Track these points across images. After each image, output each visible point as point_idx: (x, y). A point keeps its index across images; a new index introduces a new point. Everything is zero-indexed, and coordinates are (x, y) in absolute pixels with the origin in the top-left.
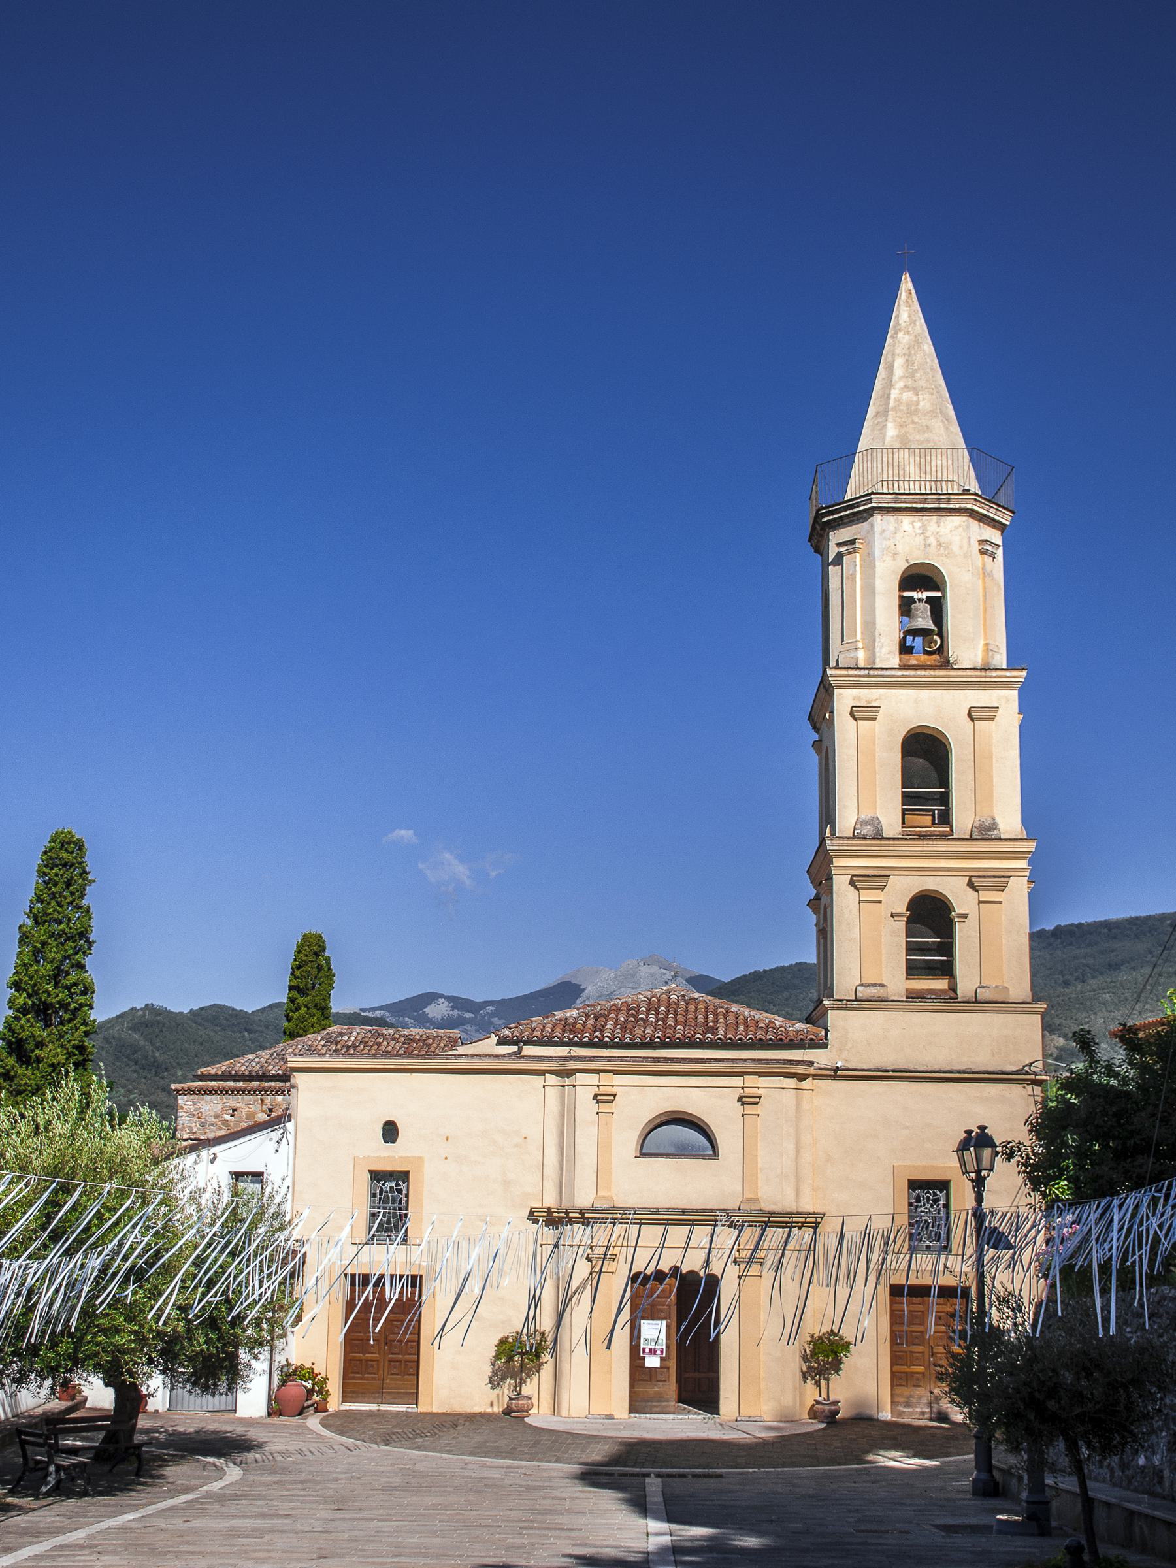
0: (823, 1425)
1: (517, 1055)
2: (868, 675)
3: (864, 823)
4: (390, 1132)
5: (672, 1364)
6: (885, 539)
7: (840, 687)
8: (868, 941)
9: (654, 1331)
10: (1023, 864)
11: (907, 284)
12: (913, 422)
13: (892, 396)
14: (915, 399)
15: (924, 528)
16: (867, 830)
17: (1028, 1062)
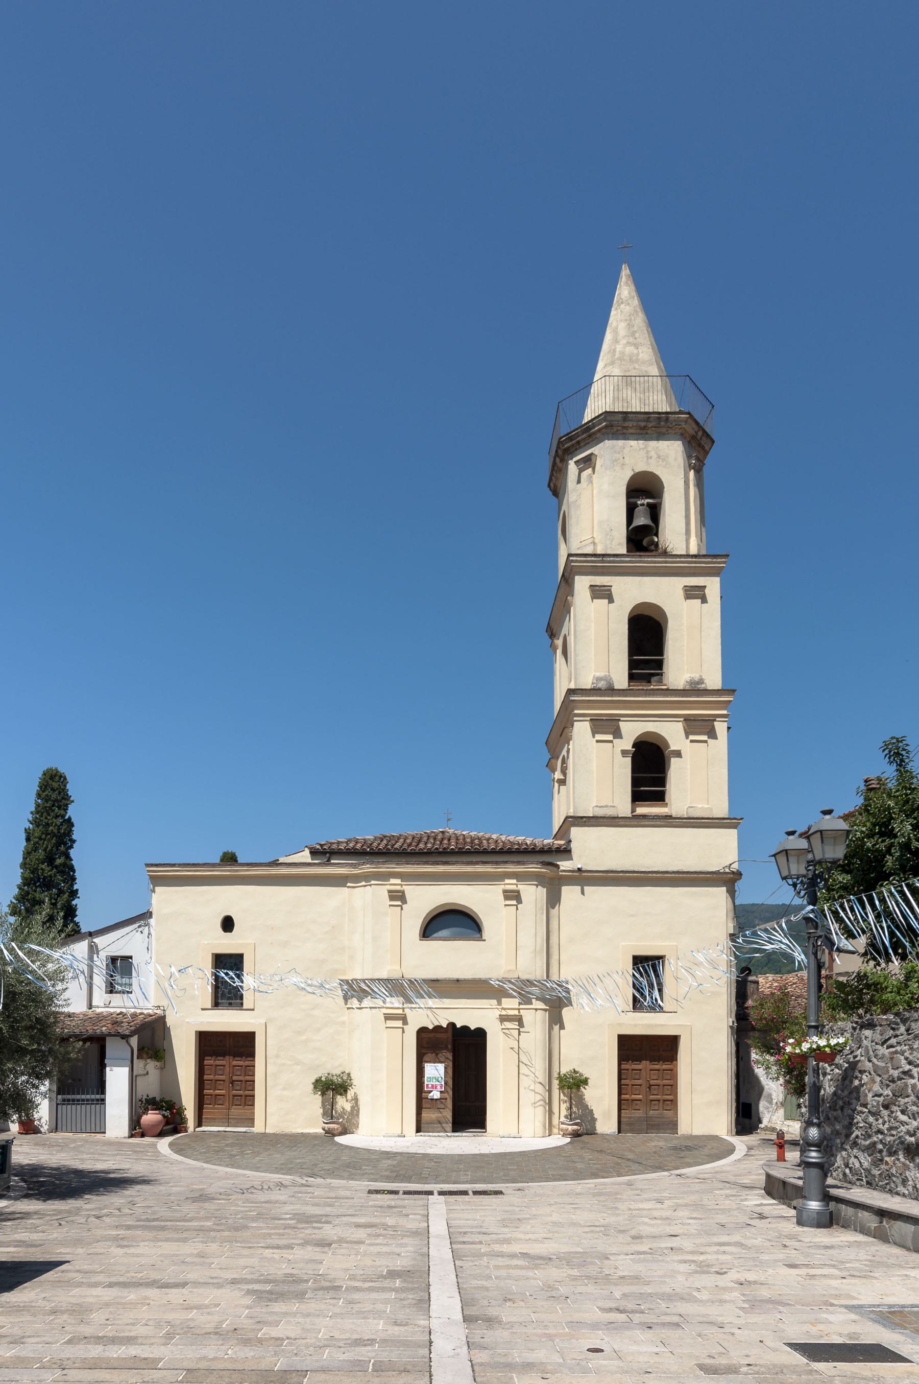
0: (568, 1140)
2: (603, 562)
3: (599, 679)
4: (228, 924)
5: (449, 1096)
6: (615, 452)
8: (596, 771)
9: (436, 1072)
11: (625, 272)
12: (635, 368)
13: (618, 350)
14: (636, 351)
16: (602, 685)
17: (728, 864)
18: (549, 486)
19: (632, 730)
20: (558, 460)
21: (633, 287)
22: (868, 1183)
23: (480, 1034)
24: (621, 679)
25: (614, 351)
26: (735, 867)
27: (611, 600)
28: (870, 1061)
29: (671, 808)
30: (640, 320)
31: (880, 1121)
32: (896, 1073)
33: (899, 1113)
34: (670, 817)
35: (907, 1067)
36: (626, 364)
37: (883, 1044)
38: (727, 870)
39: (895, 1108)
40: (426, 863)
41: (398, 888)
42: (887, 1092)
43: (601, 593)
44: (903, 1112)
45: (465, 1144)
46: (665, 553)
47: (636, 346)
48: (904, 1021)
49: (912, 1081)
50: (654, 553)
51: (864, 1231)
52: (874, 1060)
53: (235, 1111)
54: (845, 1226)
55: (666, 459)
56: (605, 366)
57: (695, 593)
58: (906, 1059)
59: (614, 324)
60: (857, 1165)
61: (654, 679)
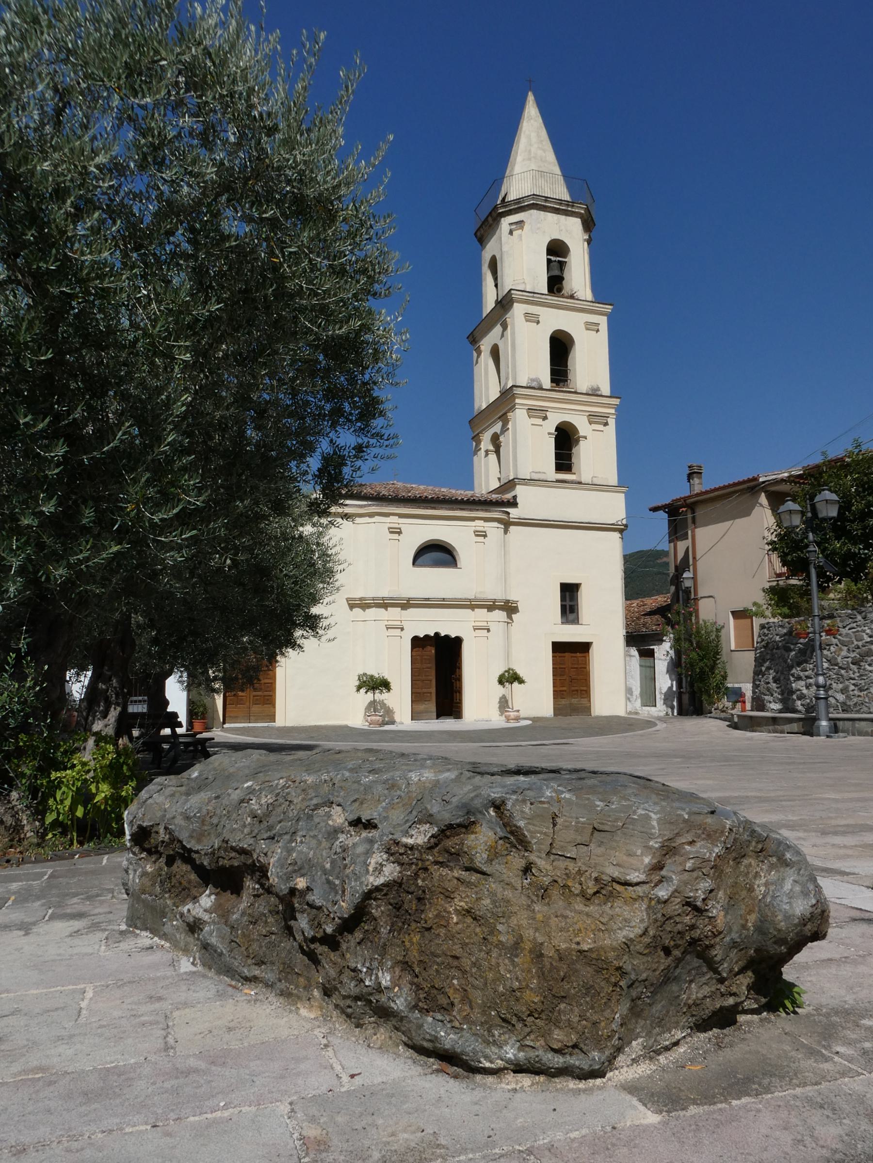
2: (533, 297)
3: (533, 380)
8: (529, 443)
11: (531, 97)
16: (534, 384)
18: (475, 234)
19: (554, 420)
20: (490, 219)
22: (843, 711)
23: (458, 641)
24: (547, 383)
25: (530, 151)
26: (624, 522)
27: (538, 322)
30: (544, 133)
31: (851, 672)
33: (867, 666)
34: (580, 483)
36: (532, 160)
37: (844, 627)
38: (620, 523)
39: (862, 664)
40: (419, 507)
41: (396, 526)
45: (448, 724)
46: (572, 297)
47: (544, 151)
48: (860, 613)
50: (558, 294)
53: (256, 709)
55: (571, 231)
56: (524, 160)
57: (592, 327)
61: (561, 384)
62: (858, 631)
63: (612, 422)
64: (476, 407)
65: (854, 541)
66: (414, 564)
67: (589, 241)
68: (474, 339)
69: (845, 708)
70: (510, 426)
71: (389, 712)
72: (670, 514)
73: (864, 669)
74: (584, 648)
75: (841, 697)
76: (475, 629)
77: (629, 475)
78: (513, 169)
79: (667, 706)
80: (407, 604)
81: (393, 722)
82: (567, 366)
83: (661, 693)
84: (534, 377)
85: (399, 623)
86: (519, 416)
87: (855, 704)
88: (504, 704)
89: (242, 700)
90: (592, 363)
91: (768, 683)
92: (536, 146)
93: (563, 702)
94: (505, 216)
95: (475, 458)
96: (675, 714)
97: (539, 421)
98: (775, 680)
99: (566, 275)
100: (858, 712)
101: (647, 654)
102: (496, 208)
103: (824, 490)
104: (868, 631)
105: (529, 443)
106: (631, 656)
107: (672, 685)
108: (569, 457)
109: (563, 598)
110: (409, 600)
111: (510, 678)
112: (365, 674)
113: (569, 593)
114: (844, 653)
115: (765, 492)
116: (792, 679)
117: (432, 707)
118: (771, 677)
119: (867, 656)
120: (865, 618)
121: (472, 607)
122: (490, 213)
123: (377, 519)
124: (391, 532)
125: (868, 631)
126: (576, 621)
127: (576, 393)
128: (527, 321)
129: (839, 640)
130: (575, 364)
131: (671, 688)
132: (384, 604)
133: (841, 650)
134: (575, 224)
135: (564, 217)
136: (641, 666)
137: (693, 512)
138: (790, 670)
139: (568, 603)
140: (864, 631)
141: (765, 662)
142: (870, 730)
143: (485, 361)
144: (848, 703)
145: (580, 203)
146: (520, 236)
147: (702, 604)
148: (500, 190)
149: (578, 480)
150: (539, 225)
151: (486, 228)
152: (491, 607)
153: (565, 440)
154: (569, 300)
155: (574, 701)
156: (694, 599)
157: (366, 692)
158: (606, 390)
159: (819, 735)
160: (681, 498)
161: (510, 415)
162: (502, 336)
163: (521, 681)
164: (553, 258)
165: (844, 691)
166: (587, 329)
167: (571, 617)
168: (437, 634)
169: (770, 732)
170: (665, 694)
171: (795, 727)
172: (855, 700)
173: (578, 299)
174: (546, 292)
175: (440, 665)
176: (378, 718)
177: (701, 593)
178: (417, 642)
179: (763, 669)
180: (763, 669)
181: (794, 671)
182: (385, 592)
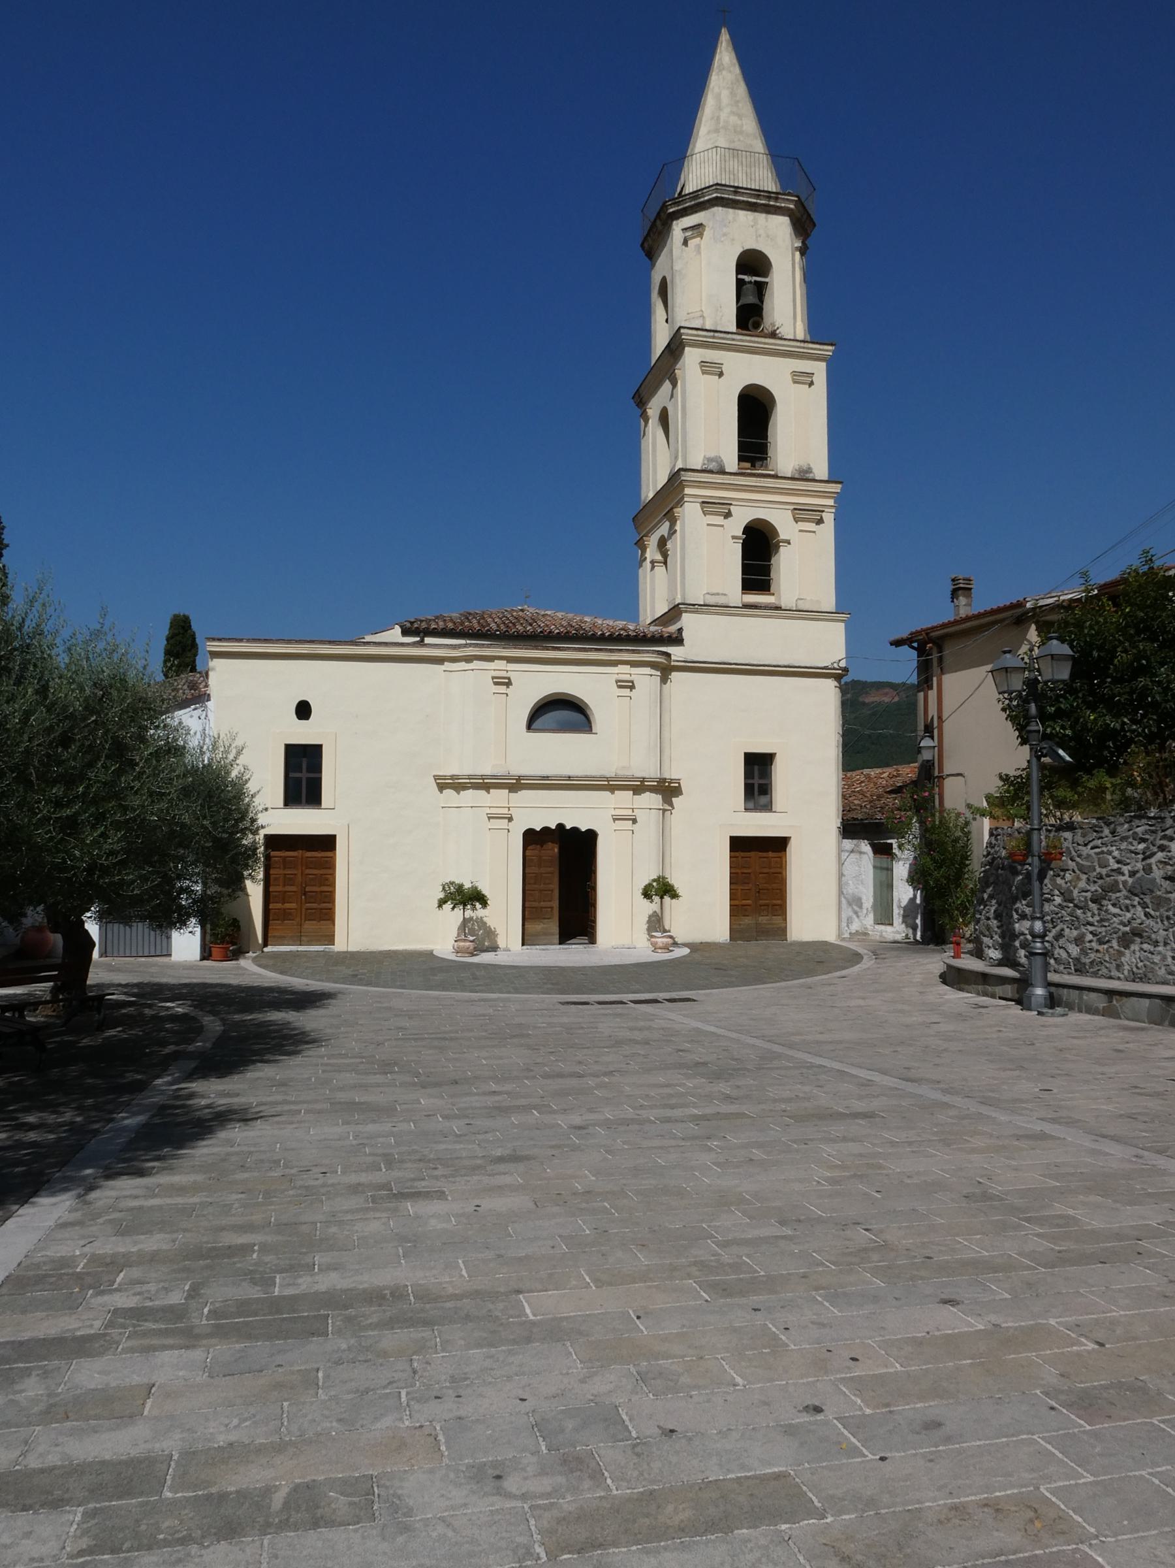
1: (421, 643)
2: (714, 337)
3: (710, 460)
4: (303, 710)
7: (690, 346)
8: (705, 552)
10: (831, 502)
11: (725, 37)
14: (739, 122)
15: (756, 222)
16: (713, 466)
18: (642, 245)
20: (658, 223)
21: (733, 55)
22: (1076, 970)
23: (591, 836)
24: (731, 460)
25: (718, 118)
26: (843, 664)
27: (721, 374)
28: (1072, 860)
29: (779, 598)
30: (742, 89)
31: (1089, 914)
32: (1104, 871)
33: (1110, 907)
34: (778, 608)
35: (1116, 866)
36: (725, 132)
37: (1086, 845)
38: (836, 665)
39: (1105, 902)
40: (536, 648)
41: (504, 674)
42: (1093, 888)
43: (713, 370)
44: (1114, 905)
45: (574, 955)
46: (773, 335)
47: (740, 116)
48: (1108, 824)
49: (1123, 878)
51: (1091, 1010)
52: (1078, 859)
53: (309, 926)
54: (1070, 1007)
55: (775, 236)
56: (709, 132)
57: (803, 379)
58: (1114, 858)
59: (716, 90)
60: (1064, 955)
61: (758, 464)
62: (1103, 852)
63: (829, 518)
64: (643, 498)
65: (1117, 710)
66: (529, 727)
67: (803, 251)
68: (641, 400)
69: (1079, 967)
70: (678, 527)
71: (490, 934)
72: (921, 651)
73: (1106, 911)
74: (779, 845)
75: (1075, 950)
76: (615, 820)
77: (853, 597)
78: (693, 149)
79: (907, 926)
80: (516, 784)
81: (494, 948)
82: (766, 437)
83: (899, 907)
84: (712, 454)
85: (505, 811)
86: (690, 513)
87: (1092, 963)
88: (656, 923)
89: (290, 914)
90: (802, 431)
91: (988, 919)
92: (727, 110)
93: (747, 921)
94: (677, 218)
95: (641, 570)
96: (918, 938)
97: (719, 520)
98: (998, 916)
99: (766, 306)
100: (1095, 975)
101: (883, 850)
102: (664, 207)
103: (1051, 638)
104: (1116, 853)
105: (705, 552)
106: (861, 853)
107: (915, 896)
108: (766, 571)
109: (748, 774)
110: (519, 778)
111: (662, 889)
112: (452, 883)
113: (758, 770)
114: (1082, 884)
115: (1036, 623)
116: (1016, 916)
117: (554, 927)
118: (993, 909)
119: (1111, 891)
120: (1113, 832)
121: (612, 789)
122: (659, 214)
123: (476, 664)
124: (496, 684)
125: (1116, 853)
126: (768, 807)
127: (776, 477)
128: (704, 373)
129: (1078, 864)
130: (776, 434)
131: (913, 900)
132: (484, 784)
133: (1079, 879)
134: (780, 226)
135: (764, 215)
136: (875, 867)
137: (940, 650)
138: (1014, 903)
139: (756, 781)
140: (1110, 853)
141: (988, 887)
142: (1101, 1006)
143: (653, 429)
144: (1083, 960)
145: (789, 194)
146: (698, 247)
147: (948, 783)
148: (679, 178)
149: (778, 604)
150: (725, 230)
151: (653, 241)
152: (639, 787)
153: (759, 547)
154: (767, 340)
155: (763, 919)
156: (938, 777)
157: (453, 908)
158: (821, 470)
159: (1029, 1009)
160: (923, 630)
161: (677, 511)
162: (672, 396)
163: (674, 895)
164: (746, 278)
165: (1079, 941)
166: (795, 382)
167: (763, 800)
168: (561, 826)
169: (978, 994)
170: (905, 909)
171: (1008, 990)
172: (1093, 956)
173: (781, 339)
174: (734, 329)
175: (563, 872)
176: (468, 944)
177: (947, 769)
178: (531, 838)
179: (986, 896)
180: (986, 896)
181: (1018, 905)
182: (487, 768)
